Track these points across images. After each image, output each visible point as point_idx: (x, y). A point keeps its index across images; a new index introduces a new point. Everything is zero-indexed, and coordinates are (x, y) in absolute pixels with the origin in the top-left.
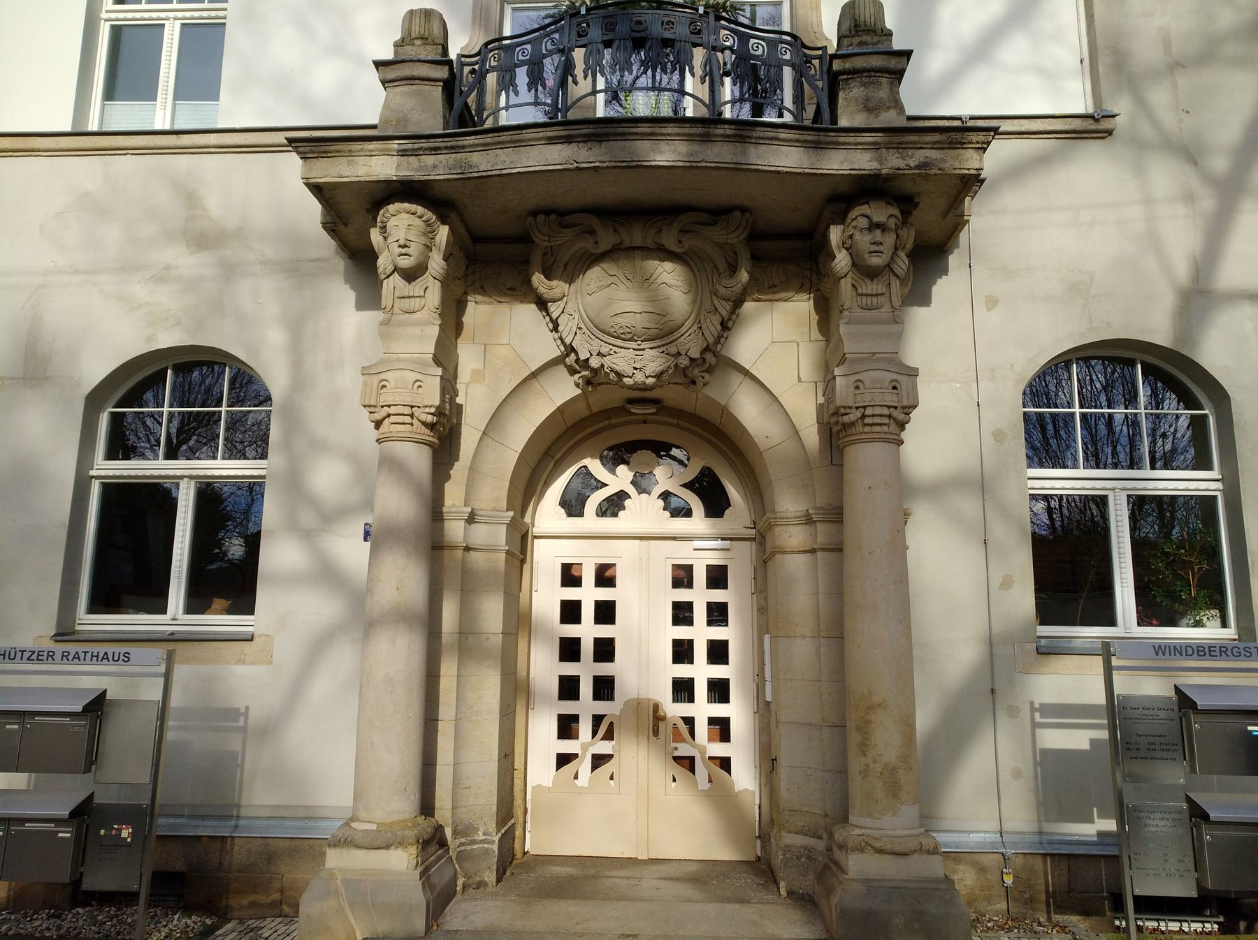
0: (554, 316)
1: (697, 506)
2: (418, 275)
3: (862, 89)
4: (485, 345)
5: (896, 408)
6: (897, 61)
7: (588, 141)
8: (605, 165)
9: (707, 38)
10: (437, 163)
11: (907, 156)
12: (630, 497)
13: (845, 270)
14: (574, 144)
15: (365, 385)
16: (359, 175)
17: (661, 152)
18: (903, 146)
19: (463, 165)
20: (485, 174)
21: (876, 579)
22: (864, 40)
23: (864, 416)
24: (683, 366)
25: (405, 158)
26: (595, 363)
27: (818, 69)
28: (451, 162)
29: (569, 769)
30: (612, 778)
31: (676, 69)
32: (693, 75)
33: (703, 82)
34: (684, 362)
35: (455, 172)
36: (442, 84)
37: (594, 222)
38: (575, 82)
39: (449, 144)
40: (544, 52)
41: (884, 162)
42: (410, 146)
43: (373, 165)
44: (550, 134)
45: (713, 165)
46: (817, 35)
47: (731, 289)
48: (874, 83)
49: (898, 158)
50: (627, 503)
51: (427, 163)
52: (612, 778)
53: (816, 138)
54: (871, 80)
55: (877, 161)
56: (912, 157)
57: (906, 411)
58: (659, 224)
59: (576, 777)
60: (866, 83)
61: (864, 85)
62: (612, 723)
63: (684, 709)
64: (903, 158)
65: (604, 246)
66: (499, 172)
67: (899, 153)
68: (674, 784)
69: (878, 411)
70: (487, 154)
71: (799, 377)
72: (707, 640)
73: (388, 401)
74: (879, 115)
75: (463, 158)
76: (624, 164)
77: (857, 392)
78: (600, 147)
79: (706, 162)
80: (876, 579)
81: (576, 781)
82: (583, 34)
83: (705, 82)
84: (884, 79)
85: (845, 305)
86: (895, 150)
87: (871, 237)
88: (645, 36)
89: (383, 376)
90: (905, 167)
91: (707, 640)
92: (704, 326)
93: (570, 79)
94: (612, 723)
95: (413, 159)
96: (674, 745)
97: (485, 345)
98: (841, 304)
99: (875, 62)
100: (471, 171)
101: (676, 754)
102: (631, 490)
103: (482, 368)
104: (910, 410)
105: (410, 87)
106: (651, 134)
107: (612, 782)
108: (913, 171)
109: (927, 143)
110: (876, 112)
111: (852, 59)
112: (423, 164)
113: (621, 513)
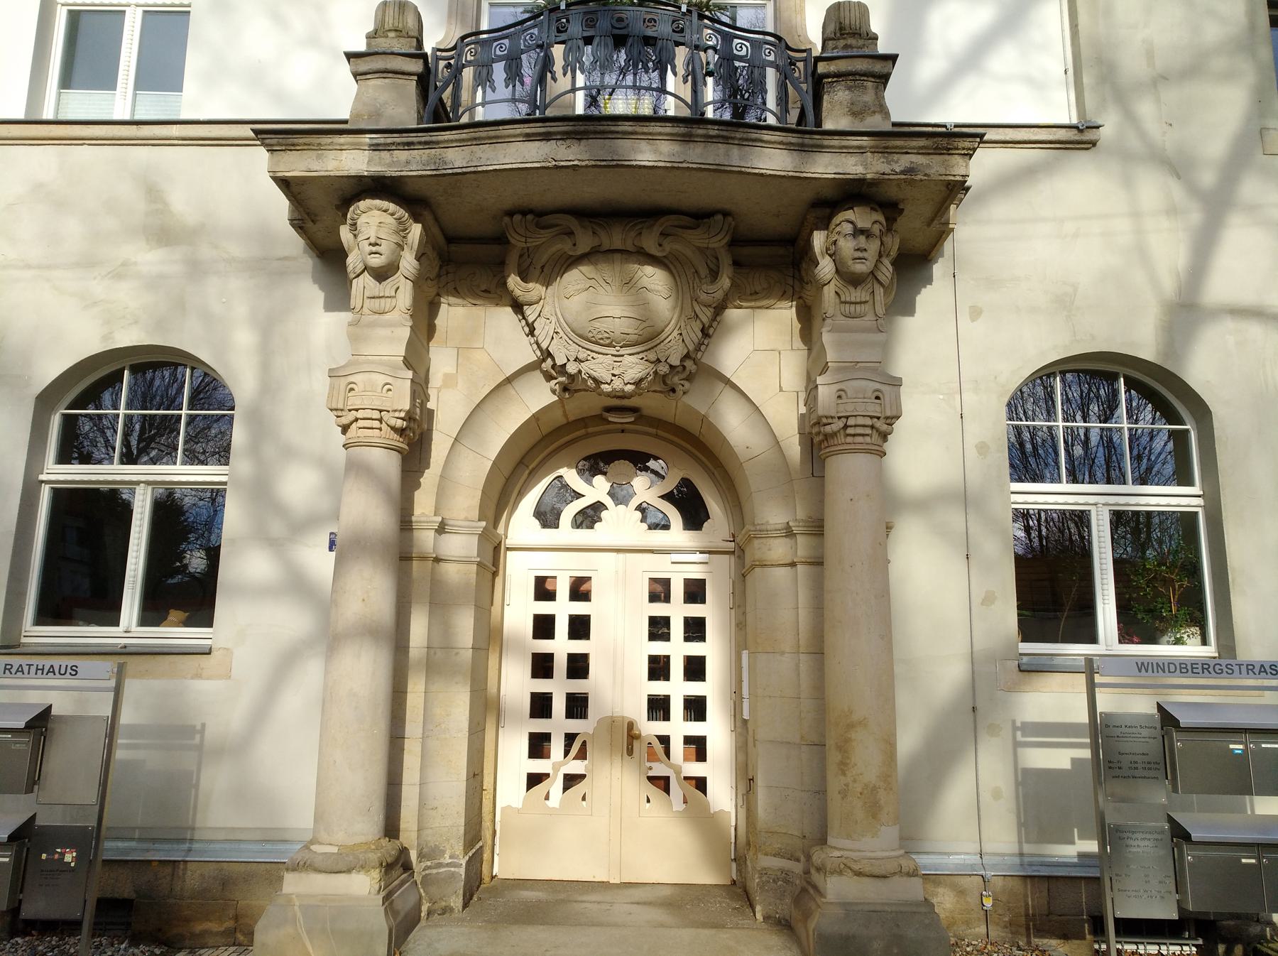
17: (641, 152)
21: (857, 594)
22: (849, 44)
28: (425, 158)
29: (540, 789)
33: (685, 81)
36: (416, 78)
38: (554, 79)
47: (712, 295)
50: (604, 514)
56: (897, 162)
57: (888, 421)
63: (660, 728)
64: (888, 163)
66: (475, 169)
69: (860, 421)
75: (437, 154)
81: (546, 802)
82: (563, 29)
83: (687, 81)
85: (829, 312)
88: (626, 33)
89: (351, 379)
93: (549, 75)
95: (385, 154)
100: (446, 167)
101: (651, 774)
102: (608, 501)
103: (455, 372)
107: (584, 803)
111: (837, 61)
112: (395, 159)
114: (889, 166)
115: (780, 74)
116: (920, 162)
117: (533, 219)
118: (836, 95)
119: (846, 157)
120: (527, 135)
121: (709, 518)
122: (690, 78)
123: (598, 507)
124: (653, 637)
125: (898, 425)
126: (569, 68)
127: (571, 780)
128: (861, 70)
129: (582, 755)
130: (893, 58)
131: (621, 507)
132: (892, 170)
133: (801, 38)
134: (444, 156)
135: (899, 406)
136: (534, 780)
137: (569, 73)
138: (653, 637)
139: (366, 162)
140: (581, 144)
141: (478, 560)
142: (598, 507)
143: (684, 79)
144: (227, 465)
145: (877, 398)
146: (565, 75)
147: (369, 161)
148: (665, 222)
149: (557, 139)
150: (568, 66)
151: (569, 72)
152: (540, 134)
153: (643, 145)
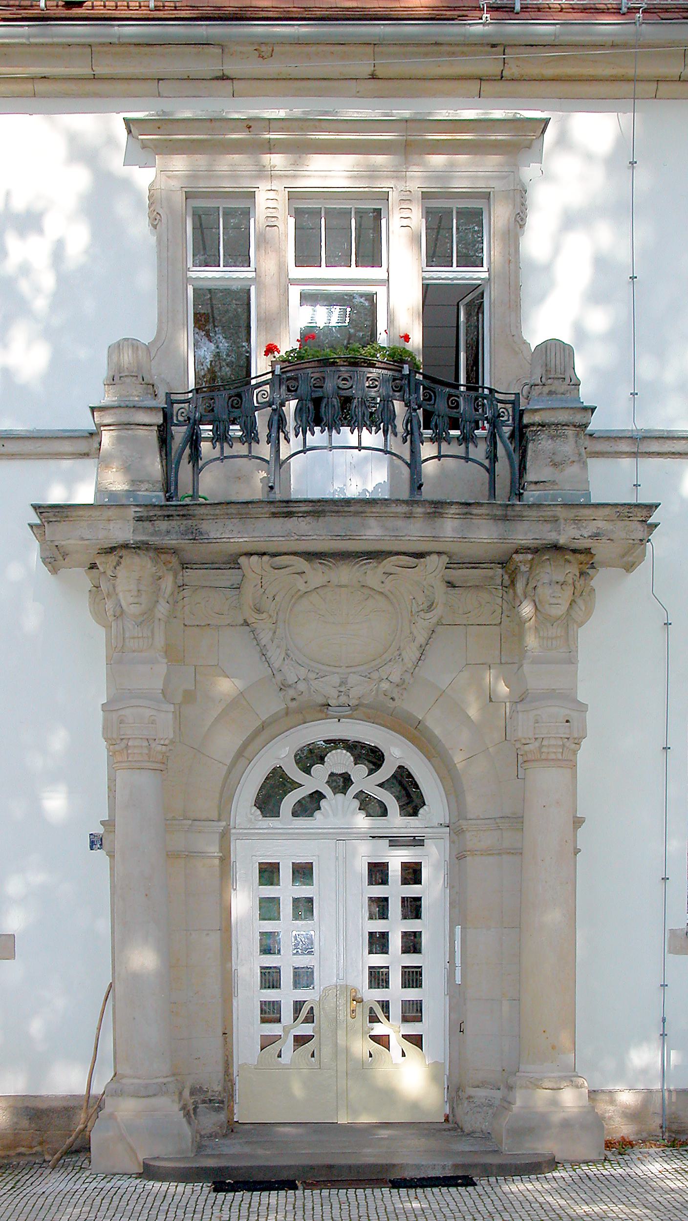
0: (263, 642)
1: (393, 805)
2: (373, 865)
3: (550, 442)
4: (195, 666)
5: (568, 739)
6: (583, 416)
7: (307, 516)
8: (321, 538)
9: (407, 396)
10: (170, 528)
11: (583, 526)
12: (325, 797)
13: (531, 615)
14: (294, 518)
15: (106, 720)
16: (99, 538)
17: (370, 528)
18: (579, 518)
19: (194, 531)
20: (214, 541)
21: (546, 882)
22: (553, 390)
23: (541, 747)
24: (384, 689)
25: (141, 522)
26: (302, 686)
27: (511, 413)
28: (183, 528)
29: (273, 1049)
30: (313, 1056)
31: (380, 429)
32: (396, 435)
33: (405, 441)
34: (385, 686)
35: (187, 538)
36: (156, 428)
37: (301, 564)
38: (288, 440)
39: (181, 513)
40: (256, 405)
41: (562, 532)
42: (145, 514)
43: (112, 528)
44: (274, 510)
45: (415, 539)
46: (515, 338)
47: (429, 621)
48: (560, 436)
49: (574, 528)
50: (323, 803)
51: (161, 528)
52: (313, 1056)
53: (504, 512)
54: (558, 432)
55: (556, 531)
56: (585, 528)
57: (576, 741)
58: (365, 567)
59: (279, 1056)
60: (554, 436)
61: (552, 437)
62: (312, 1008)
63: (379, 994)
64: (579, 529)
65: (201, 291)
66: (228, 540)
67: (575, 524)
68: (370, 1059)
69: (552, 742)
70: (216, 523)
71: (490, 697)
72: (278, 884)
73: (127, 735)
74: (564, 470)
75: (194, 525)
76: (339, 538)
77: (537, 725)
78: (317, 522)
79: (409, 536)
80: (546, 882)
81: (280, 1059)
82: (293, 389)
83: (406, 441)
84: (571, 431)
85: (529, 646)
86: (572, 521)
87: (551, 591)
88: (350, 394)
89: (121, 713)
90: (580, 537)
91: (278, 884)
92: (404, 654)
93: (282, 435)
94: (312, 1008)
95: (147, 524)
96: (369, 1025)
97: (195, 666)
98: (525, 645)
99: (562, 417)
100: (202, 537)
101: (373, 1033)
102: (327, 791)
103: (194, 688)
104: (580, 741)
105: (126, 431)
106: (362, 512)
107: (313, 1059)
108: (587, 541)
109: (598, 517)
110: (561, 467)
111: (541, 412)
112: (157, 529)
113: (317, 814)
114: (579, 532)
115: (490, 426)
116: (605, 528)
117: (269, 560)
118: (540, 443)
119: (542, 524)
120: (273, 513)
121: (425, 804)
122: (408, 437)
123: (317, 796)
124: (417, 935)
125: (584, 742)
126: (301, 428)
127: (301, 1040)
128: (563, 421)
129: (310, 1019)
130: (593, 409)
131: (340, 796)
132: (581, 536)
133: (515, 338)
134: (200, 527)
135: (584, 729)
136: (267, 1042)
137: (301, 434)
138: (417, 935)
139: (132, 531)
140: (319, 520)
141: (221, 855)
142: (317, 796)
143: (403, 439)
144: (312, 901)
145: (567, 721)
146: (297, 436)
147: (134, 530)
148: (389, 564)
149: (299, 517)
150: (299, 427)
151: (301, 433)
152: (284, 513)
153: (372, 522)
